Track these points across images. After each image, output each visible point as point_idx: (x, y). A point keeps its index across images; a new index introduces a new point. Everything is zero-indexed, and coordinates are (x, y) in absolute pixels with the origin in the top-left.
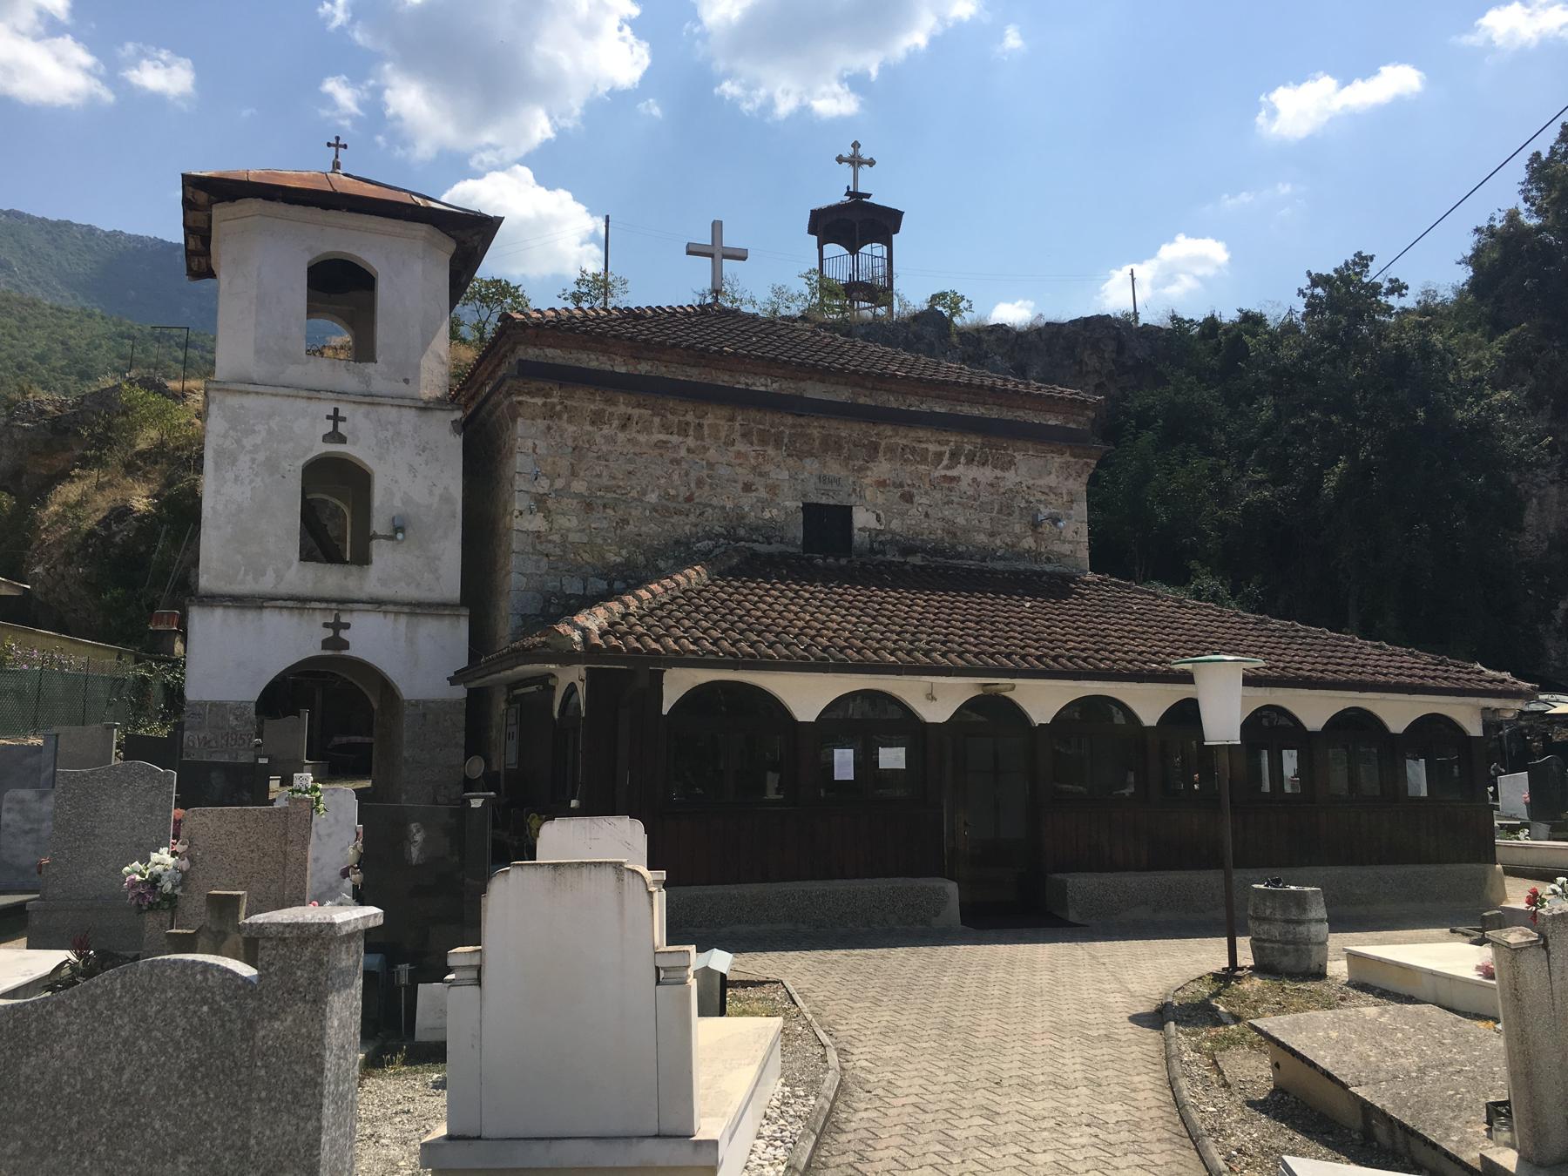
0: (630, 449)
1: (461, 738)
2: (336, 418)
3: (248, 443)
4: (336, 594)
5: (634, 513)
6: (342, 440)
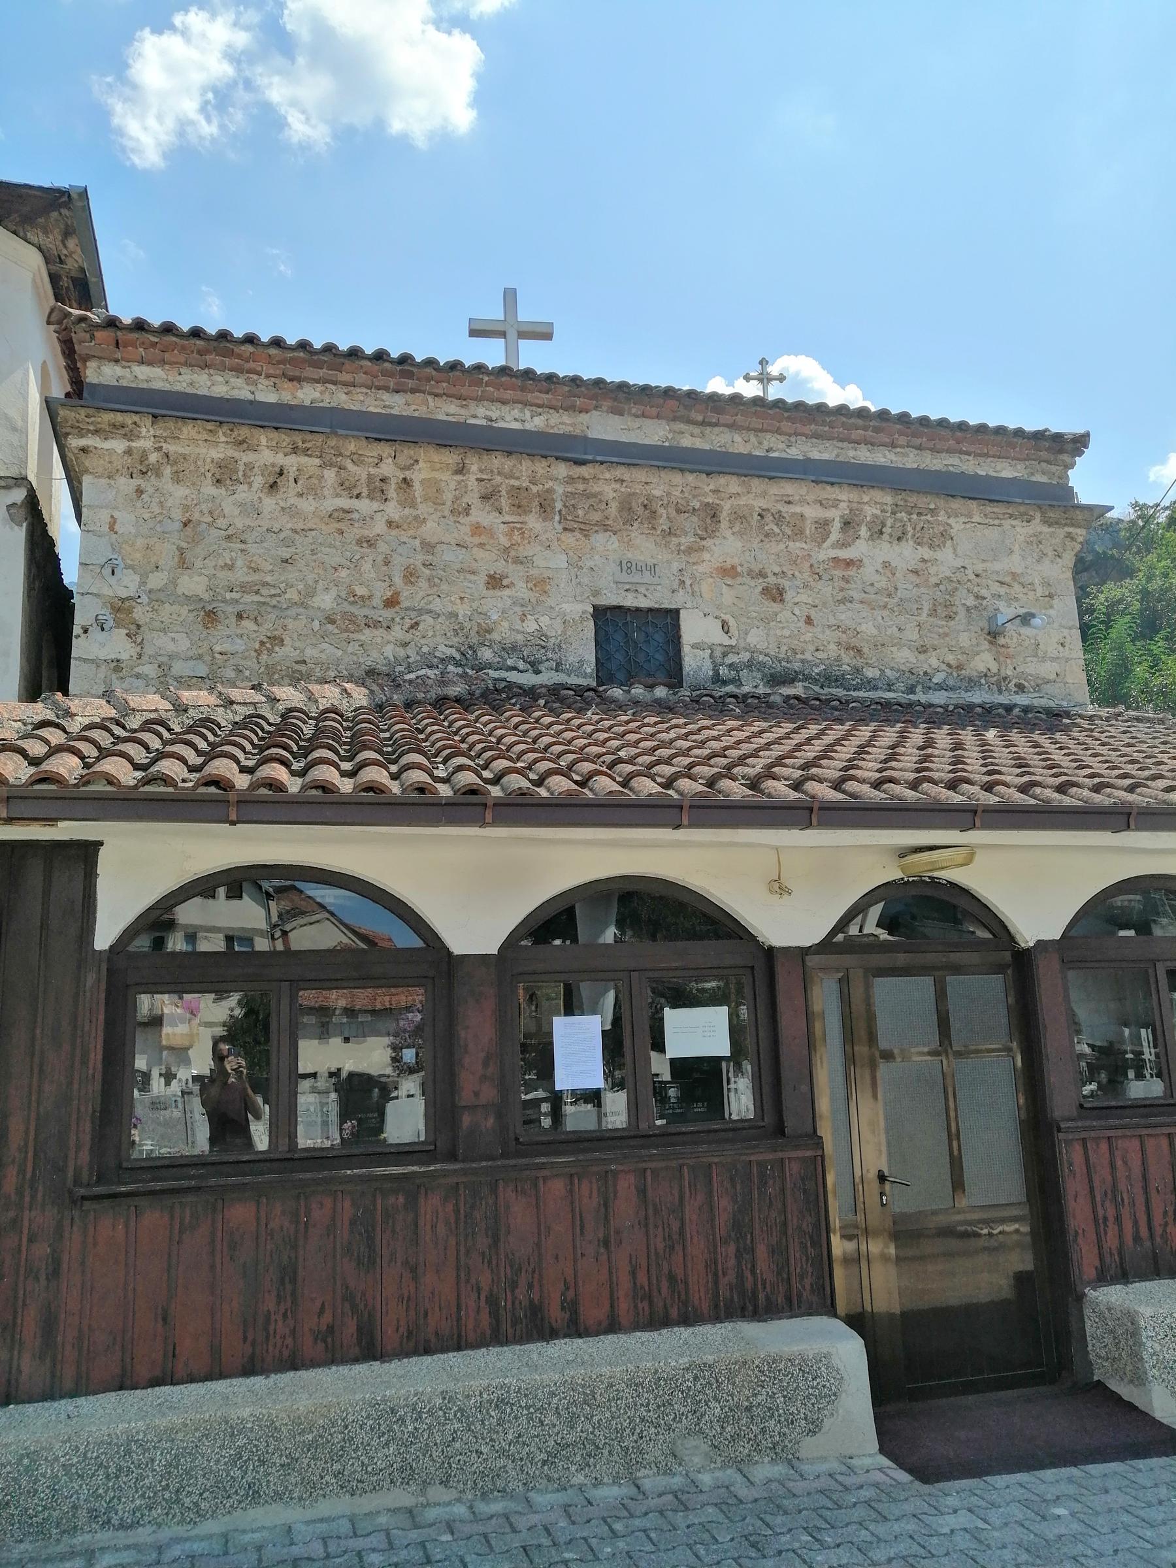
0: (286, 523)
5: (291, 625)
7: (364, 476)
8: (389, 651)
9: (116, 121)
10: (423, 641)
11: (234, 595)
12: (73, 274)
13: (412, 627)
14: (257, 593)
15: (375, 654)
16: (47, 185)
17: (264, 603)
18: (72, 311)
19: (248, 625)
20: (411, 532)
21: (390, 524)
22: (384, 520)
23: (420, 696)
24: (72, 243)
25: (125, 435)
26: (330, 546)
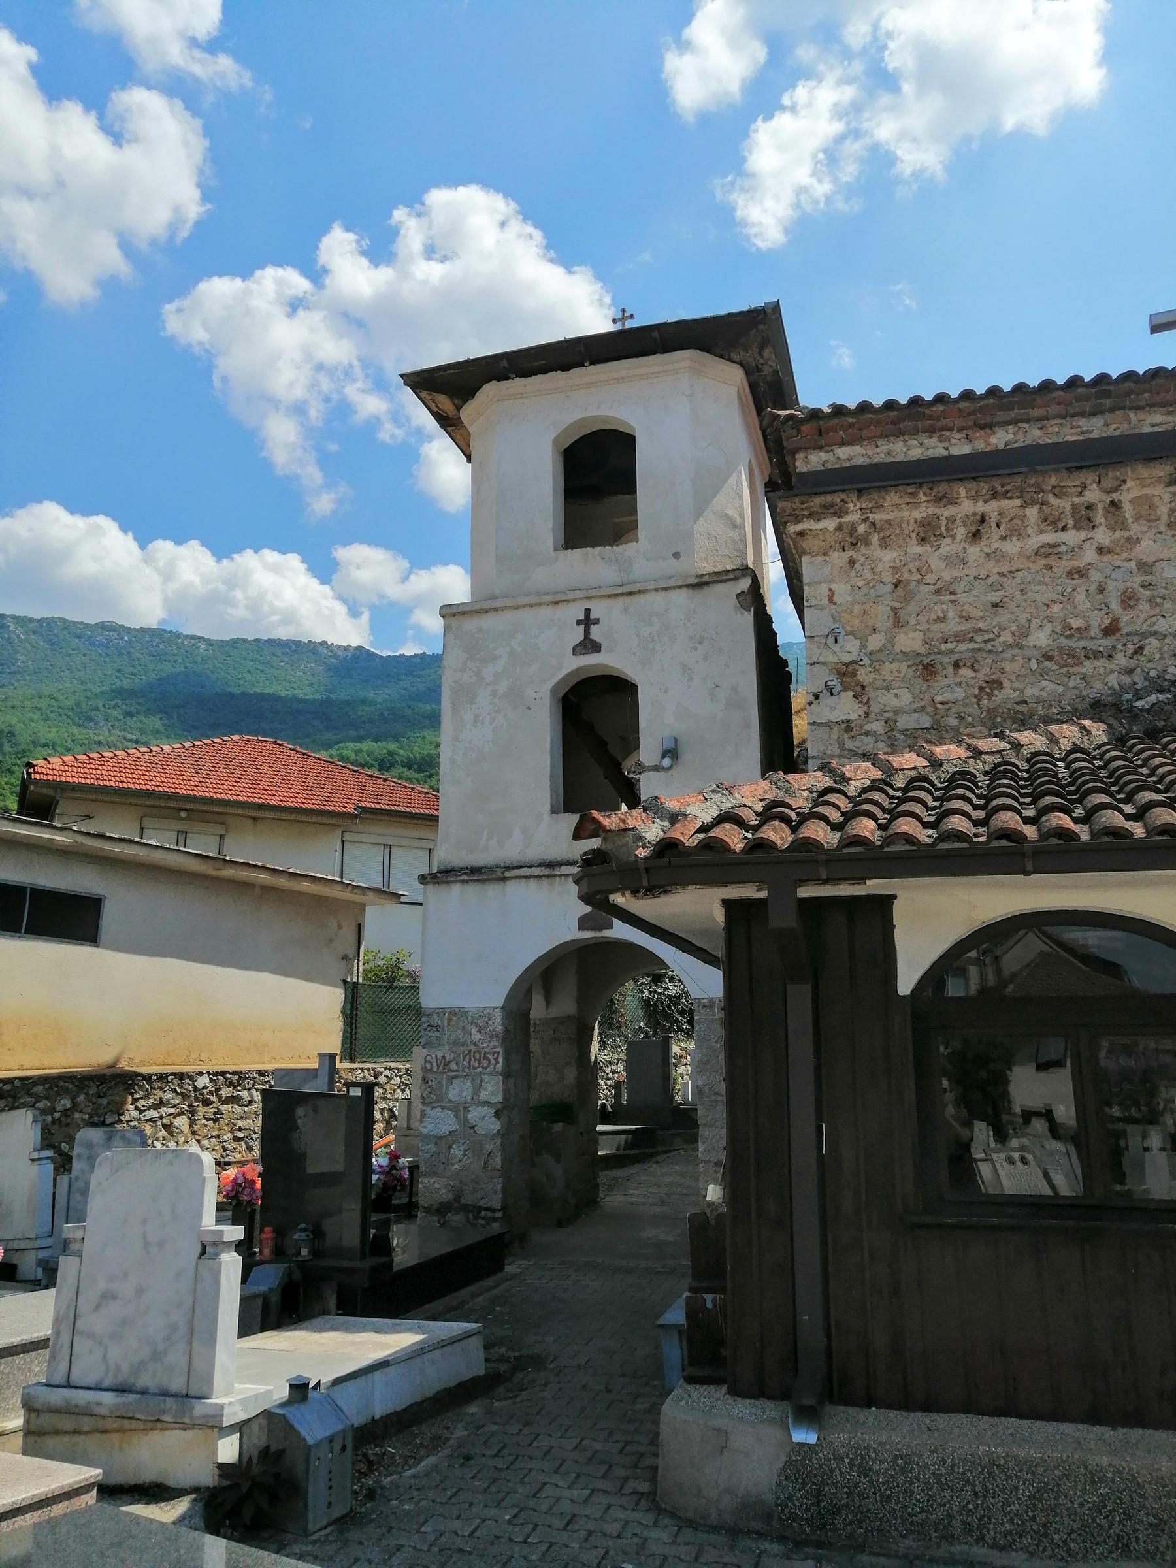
0: (993, 568)
2: (588, 621)
3: (488, 672)
5: (1008, 667)
6: (596, 648)
7: (1068, 508)
8: (1113, 680)
9: (739, 214)
10: (1148, 665)
11: (950, 646)
12: (769, 378)
13: (1136, 652)
14: (971, 640)
15: (1098, 685)
16: (745, 309)
17: (979, 650)
18: (779, 412)
19: (966, 672)
20: (1125, 555)
21: (1100, 550)
22: (1094, 548)
23: (1161, 724)
24: (767, 352)
26: (1040, 583)
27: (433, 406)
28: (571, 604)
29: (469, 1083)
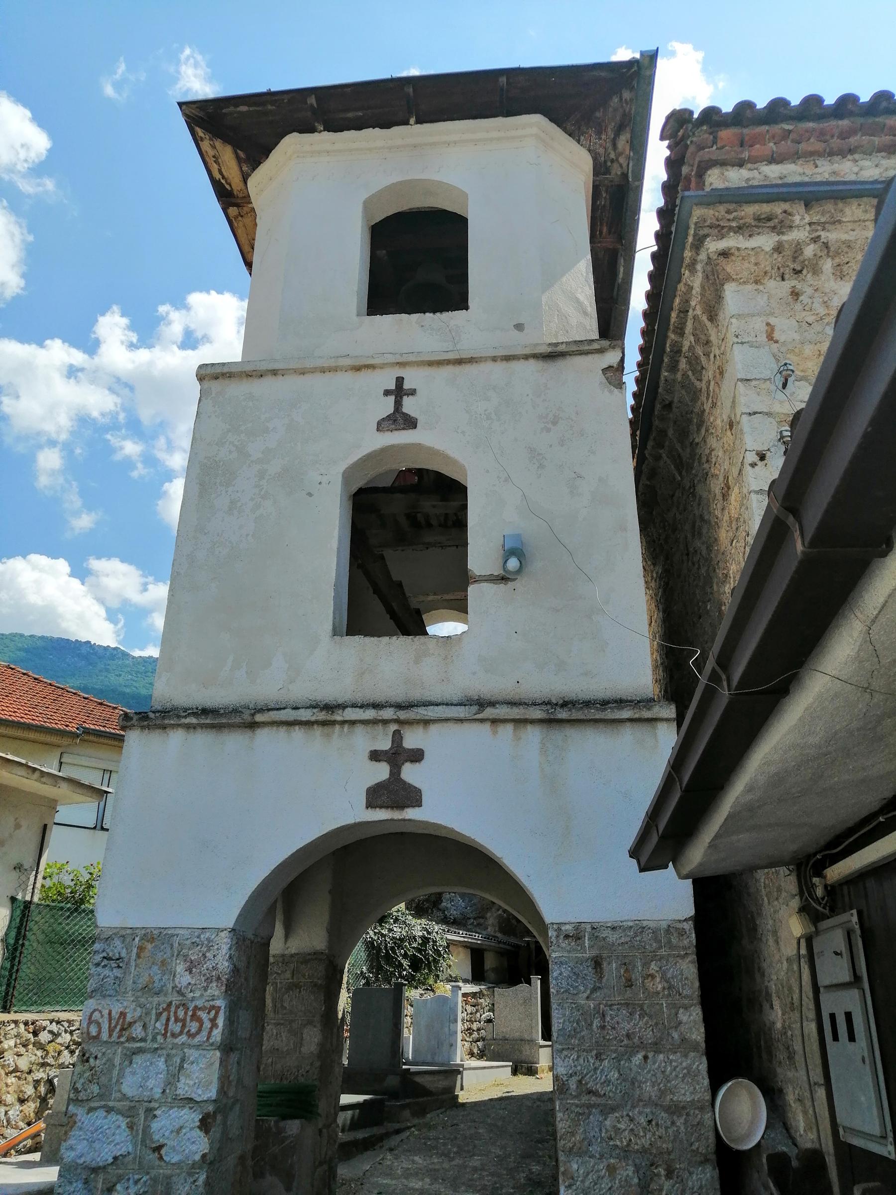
1: (692, 1023)
2: (399, 391)
4: (398, 694)
6: (410, 423)
25: (774, 228)
27: (215, 168)
28: (378, 371)
29: (161, 1064)
